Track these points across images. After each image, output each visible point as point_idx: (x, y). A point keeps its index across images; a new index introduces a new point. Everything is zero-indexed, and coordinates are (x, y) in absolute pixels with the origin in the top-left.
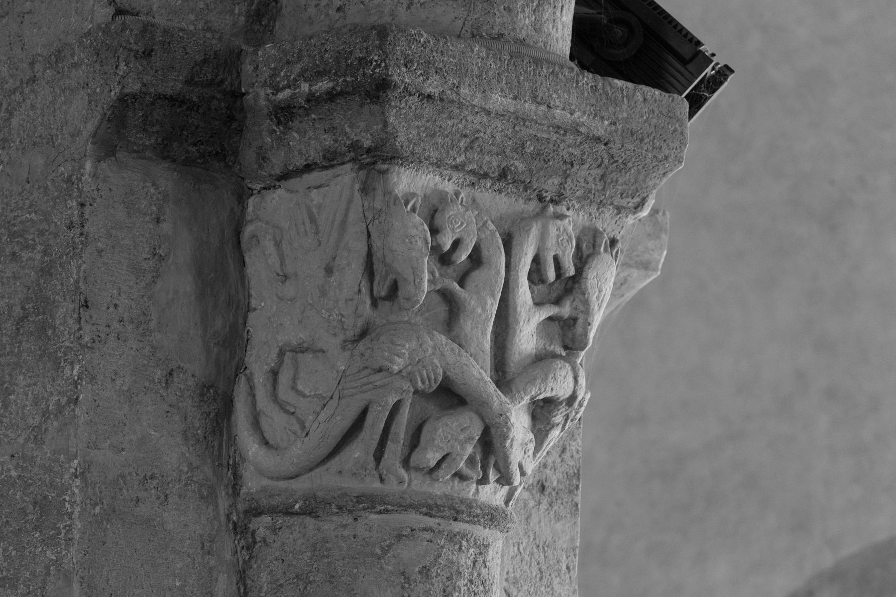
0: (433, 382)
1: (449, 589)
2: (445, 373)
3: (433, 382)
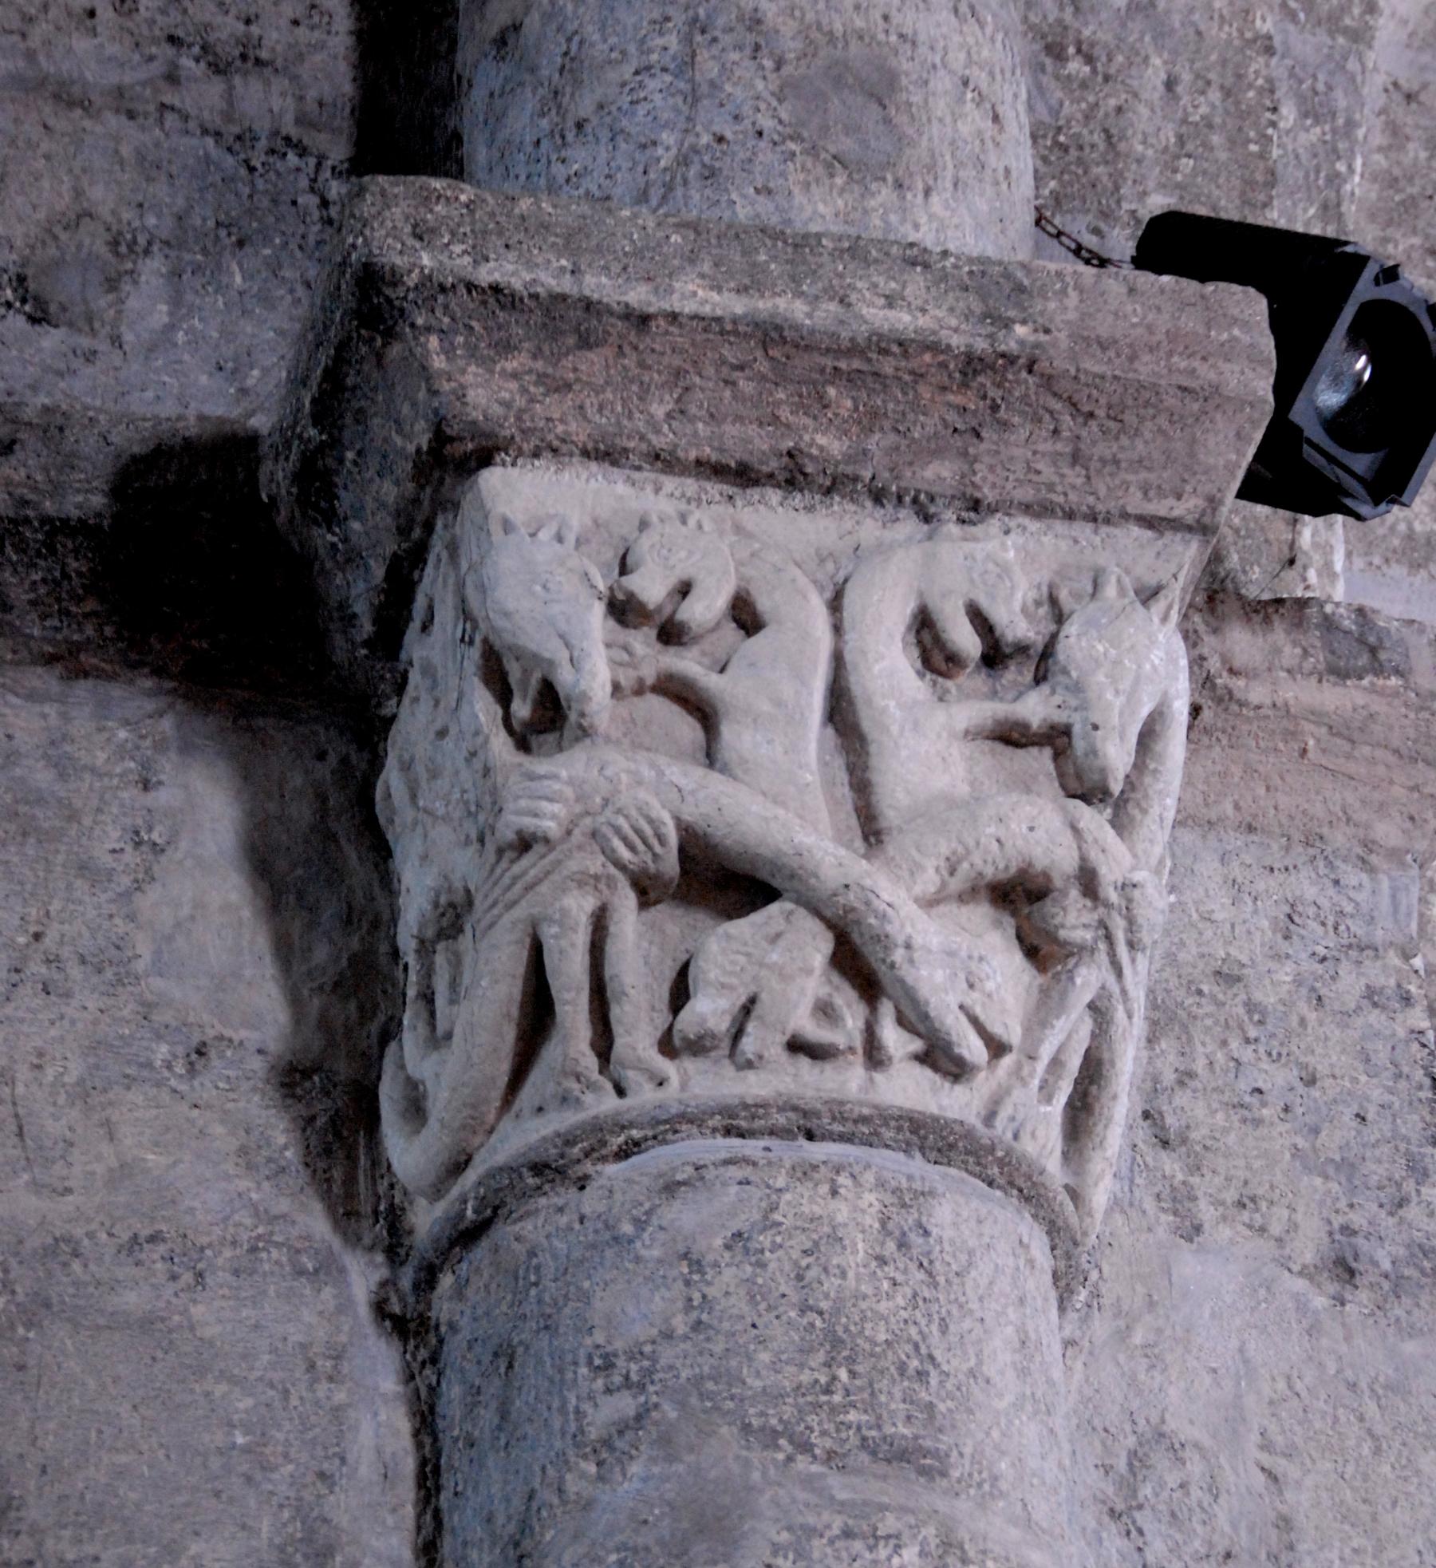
0: (655, 843)
1: (811, 1274)
2: (678, 821)
3: (655, 843)
